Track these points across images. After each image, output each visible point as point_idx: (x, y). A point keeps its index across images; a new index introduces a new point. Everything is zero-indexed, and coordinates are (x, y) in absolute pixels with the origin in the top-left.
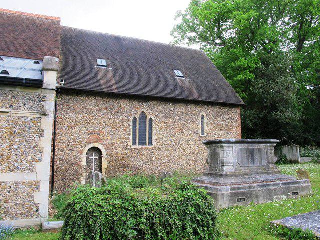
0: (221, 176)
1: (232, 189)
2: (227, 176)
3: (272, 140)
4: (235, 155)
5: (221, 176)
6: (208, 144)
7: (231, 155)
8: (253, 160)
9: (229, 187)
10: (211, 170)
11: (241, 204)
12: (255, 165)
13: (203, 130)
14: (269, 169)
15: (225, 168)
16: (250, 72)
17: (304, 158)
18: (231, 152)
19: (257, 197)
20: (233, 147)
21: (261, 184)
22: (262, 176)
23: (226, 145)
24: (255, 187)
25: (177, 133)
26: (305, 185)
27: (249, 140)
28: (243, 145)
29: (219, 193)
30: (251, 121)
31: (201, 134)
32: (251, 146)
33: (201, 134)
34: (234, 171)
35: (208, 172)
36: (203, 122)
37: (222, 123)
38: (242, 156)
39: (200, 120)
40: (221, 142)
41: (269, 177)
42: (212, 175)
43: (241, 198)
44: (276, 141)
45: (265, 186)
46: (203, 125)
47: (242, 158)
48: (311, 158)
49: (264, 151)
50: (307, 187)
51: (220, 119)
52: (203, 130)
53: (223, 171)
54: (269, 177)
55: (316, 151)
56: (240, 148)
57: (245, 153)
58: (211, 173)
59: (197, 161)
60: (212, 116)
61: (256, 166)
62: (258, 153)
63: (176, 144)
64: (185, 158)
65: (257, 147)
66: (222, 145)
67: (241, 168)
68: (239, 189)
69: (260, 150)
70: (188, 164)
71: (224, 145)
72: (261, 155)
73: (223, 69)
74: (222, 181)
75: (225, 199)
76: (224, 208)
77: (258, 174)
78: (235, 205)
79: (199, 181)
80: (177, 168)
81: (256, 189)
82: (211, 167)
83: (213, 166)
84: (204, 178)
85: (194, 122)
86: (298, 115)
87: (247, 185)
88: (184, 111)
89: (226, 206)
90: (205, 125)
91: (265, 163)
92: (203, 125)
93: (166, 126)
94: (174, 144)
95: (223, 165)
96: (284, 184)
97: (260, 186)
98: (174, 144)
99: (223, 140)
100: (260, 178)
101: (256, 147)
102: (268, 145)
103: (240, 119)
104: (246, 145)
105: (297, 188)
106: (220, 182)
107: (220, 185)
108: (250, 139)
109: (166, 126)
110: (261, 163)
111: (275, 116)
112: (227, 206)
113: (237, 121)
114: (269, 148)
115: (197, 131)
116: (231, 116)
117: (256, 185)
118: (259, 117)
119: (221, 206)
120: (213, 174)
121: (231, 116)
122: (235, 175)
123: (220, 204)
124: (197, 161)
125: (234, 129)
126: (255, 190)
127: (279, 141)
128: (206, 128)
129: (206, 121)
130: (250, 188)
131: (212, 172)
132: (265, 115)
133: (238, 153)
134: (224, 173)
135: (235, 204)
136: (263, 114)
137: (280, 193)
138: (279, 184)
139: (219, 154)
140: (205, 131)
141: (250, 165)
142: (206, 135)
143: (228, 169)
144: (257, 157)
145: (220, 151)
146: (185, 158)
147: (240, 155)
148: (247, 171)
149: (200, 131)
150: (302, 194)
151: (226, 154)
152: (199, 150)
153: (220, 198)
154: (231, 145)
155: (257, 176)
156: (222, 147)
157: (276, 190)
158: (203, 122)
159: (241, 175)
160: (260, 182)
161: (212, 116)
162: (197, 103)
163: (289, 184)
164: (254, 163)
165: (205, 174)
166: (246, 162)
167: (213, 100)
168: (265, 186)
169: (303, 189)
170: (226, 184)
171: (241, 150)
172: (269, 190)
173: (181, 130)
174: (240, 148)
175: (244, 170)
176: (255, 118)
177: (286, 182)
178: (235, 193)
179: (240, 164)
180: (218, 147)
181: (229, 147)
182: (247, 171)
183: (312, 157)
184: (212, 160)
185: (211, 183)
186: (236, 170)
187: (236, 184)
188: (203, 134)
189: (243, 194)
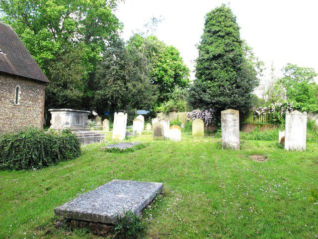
8: (79, 122)
16: (52, 54)
31: (15, 103)
36: (17, 92)
39: (16, 91)
45: (87, 136)
46: (17, 95)
73: (205, 33)
88: (4, 82)
90: (19, 95)
92: (17, 95)
96: (94, 135)
115: (13, 100)
125: (40, 101)
128: (19, 98)
140: (19, 100)
142: (19, 104)
149: (15, 100)
158: (17, 92)
162: (14, 77)
167: (28, 76)
168: (87, 136)
187: (85, 133)
188: (17, 103)
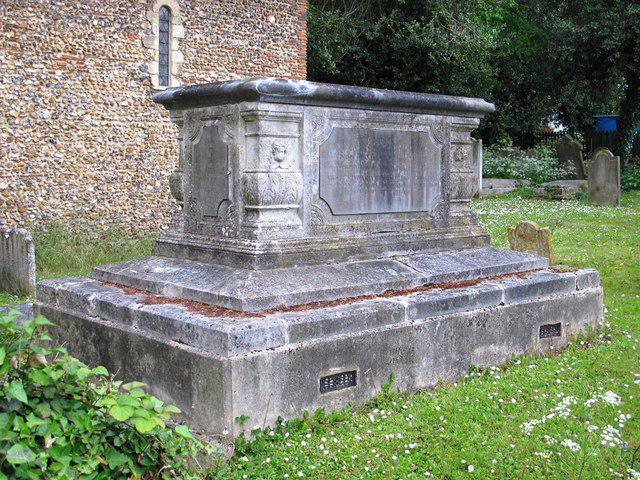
0: (243, 259)
1: (298, 332)
2: (269, 259)
3: (469, 102)
4: (311, 159)
5: (243, 259)
6: (181, 102)
7: (291, 158)
8: (387, 186)
9: (282, 321)
10: (193, 228)
11: (336, 401)
12: (396, 207)
13: (165, 65)
14: (446, 225)
15: (264, 219)
17: (495, 182)
18: (292, 146)
19: (409, 358)
20: (300, 123)
21: (425, 298)
22: (419, 254)
23: (272, 108)
24: (399, 313)
25: (59, 73)
26: (582, 294)
27: (378, 93)
28: (347, 112)
29: (235, 356)
30: (333, 46)
31: (155, 81)
32: (382, 122)
33: (155, 81)
34: (302, 233)
35: (178, 236)
36: (165, 33)
37: (239, 43)
38: (339, 164)
39: (156, 26)
40: (247, 94)
41: (446, 263)
42: (194, 251)
43: (336, 370)
44: (482, 103)
46: (165, 43)
47: (340, 175)
48: (511, 182)
49: (433, 147)
50: (591, 299)
51: (230, 28)
52: (165, 65)
53: (252, 237)
54: (446, 263)
55: (527, 158)
56: (335, 125)
57: (354, 151)
58: (191, 243)
59: (138, 184)
60: (201, 14)
61: (397, 214)
62: (408, 156)
63: (55, 117)
64: (91, 170)
65: (406, 128)
66: (251, 106)
67: (337, 223)
68: (330, 326)
69: (417, 141)
70: (105, 197)
71: (262, 107)
72: (421, 165)
74: (246, 286)
75: (265, 384)
76: (254, 432)
77: (403, 246)
78: (312, 409)
79: (132, 285)
80: (59, 210)
81: (406, 322)
82: (192, 212)
83: (201, 207)
84: (159, 267)
85: (130, 33)
86: (489, 38)
87: (366, 306)
89: (264, 419)
90: (174, 45)
91: (432, 200)
92: (165, 43)
93: (13, 39)
94: (47, 114)
95: (252, 204)
97: (422, 308)
98: (47, 114)
99: (257, 83)
100: (416, 269)
101: (400, 125)
102: (452, 120)
103: (304, 33)
104: (363, 114)
105: (557, 308)
106: (239, 295)
107: (235, 309)
108: (380, 87)
109: (13, 39)
110: (419, 200)
111: (415, 36)
112: (273, 416)
113: (292, 42)
114: (453, 136)
115: (143, 69)
116: (272, 19)
117: (404, 301)
118: (363, 37)
119: (242, 420)
120: (201, 250)
121: (272, 19)
122: (305, 257)
123: (236, 414)
124: (138, 184)
126: (403, 330)
127: (491, 106)
128: (176, 57)
129: (178, 31)
130: (381, 317)
131: (199, 241)
132: (385, 30)
133: (323, 153)
134: (258, 247)
135: (310, 401)
136: (378, 26)
137: (498, 332)
138: (495, 295)
139: (235, 155)
140: (174, 69)
141: (375, 209)
143: (275, 227)
144: (403, 173)
145: (238, 138)
146: (91, 170)
147: (333, 160)
148: (359, 236)
149: (154, 67)
150: (575, 328)
151: (266, 152)
152: (149, 139)
153: (236, 382)
154: (294, 110)
155: (402, 257)
156: (251, 118)
157: (482, 320)
158: (165, 33)
159: (331, 254)
160: (416, 284)
161: (201, 14)
163: (533, 289)
164: (390, 202)
165: (161, 248)
166: (356, 196)
168: (444, 305)
169: (579, 308)
170: (267, 306)
171: (340, 137)
172: (461, 327)
173: (75, 61)
174: (335, 125)
175: (346, 232)
176: (349, 40)
177: (521, 282)
178: (313, 352)
179: (331, 202)
180: (233, 122)
181: (285, 119)
182: (359, 236)
183: (517, 178)
184: (197, 178)
185: (191, 301)
186: (313, 228)
189: (347, 350)
